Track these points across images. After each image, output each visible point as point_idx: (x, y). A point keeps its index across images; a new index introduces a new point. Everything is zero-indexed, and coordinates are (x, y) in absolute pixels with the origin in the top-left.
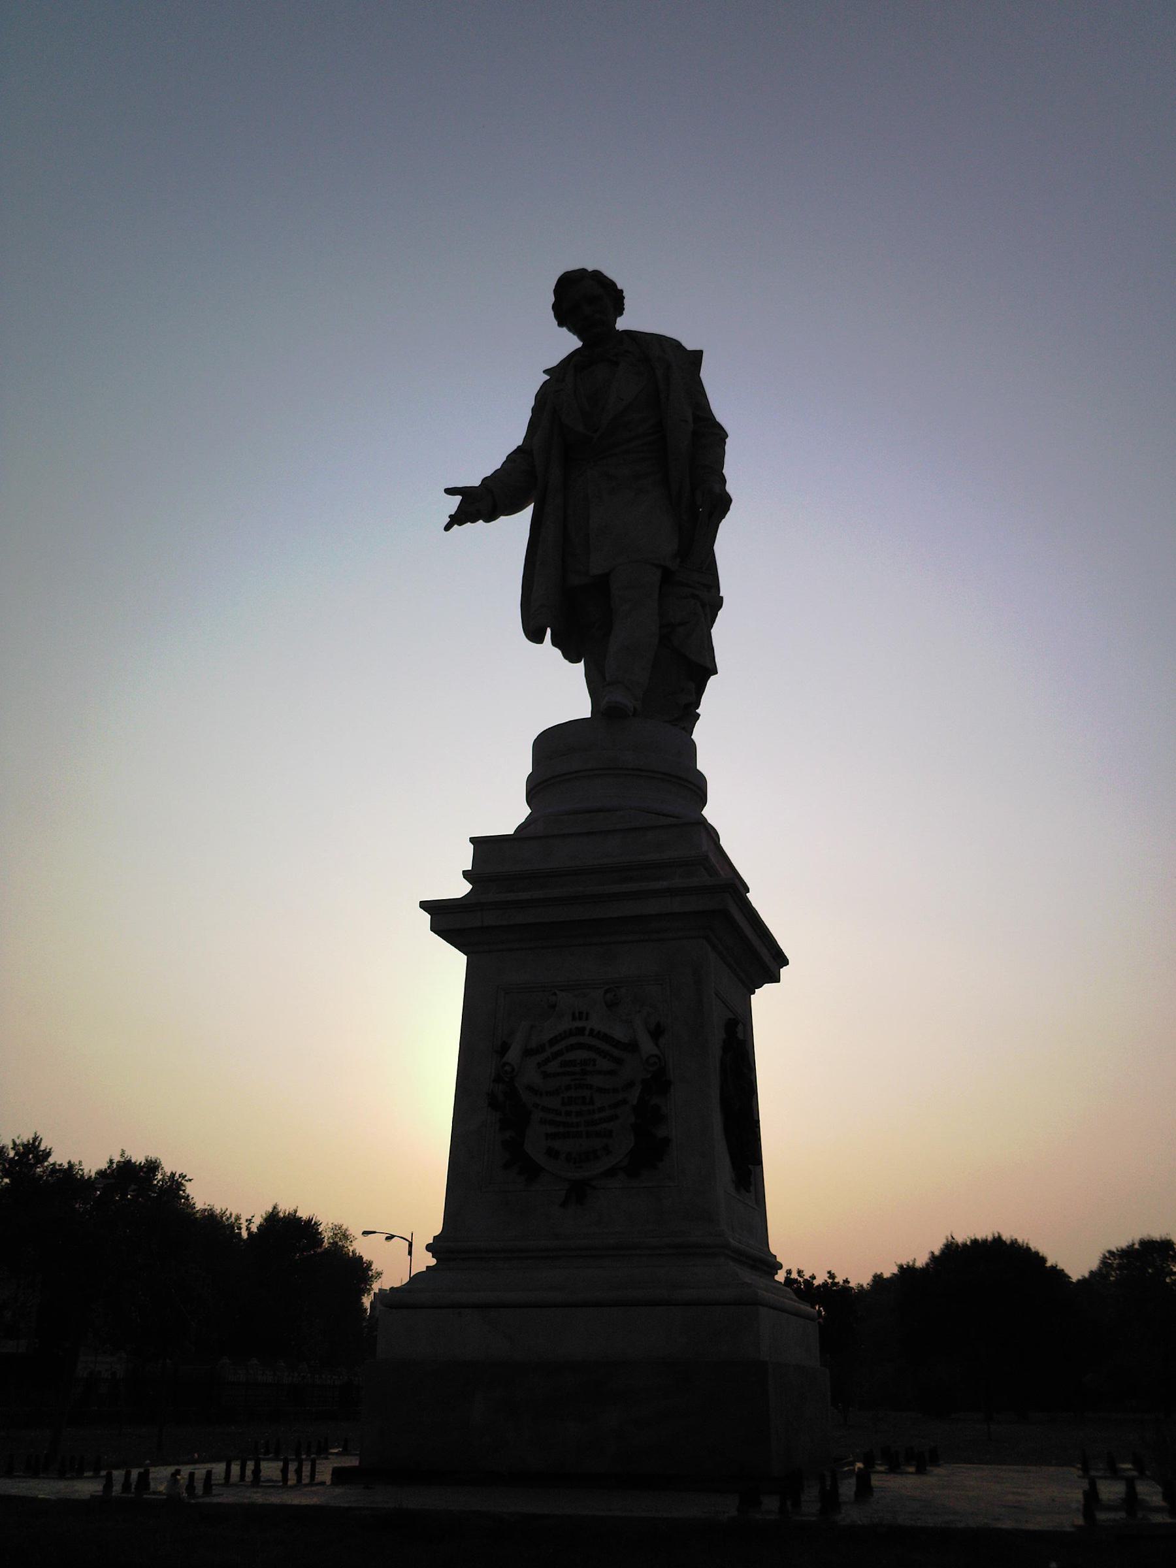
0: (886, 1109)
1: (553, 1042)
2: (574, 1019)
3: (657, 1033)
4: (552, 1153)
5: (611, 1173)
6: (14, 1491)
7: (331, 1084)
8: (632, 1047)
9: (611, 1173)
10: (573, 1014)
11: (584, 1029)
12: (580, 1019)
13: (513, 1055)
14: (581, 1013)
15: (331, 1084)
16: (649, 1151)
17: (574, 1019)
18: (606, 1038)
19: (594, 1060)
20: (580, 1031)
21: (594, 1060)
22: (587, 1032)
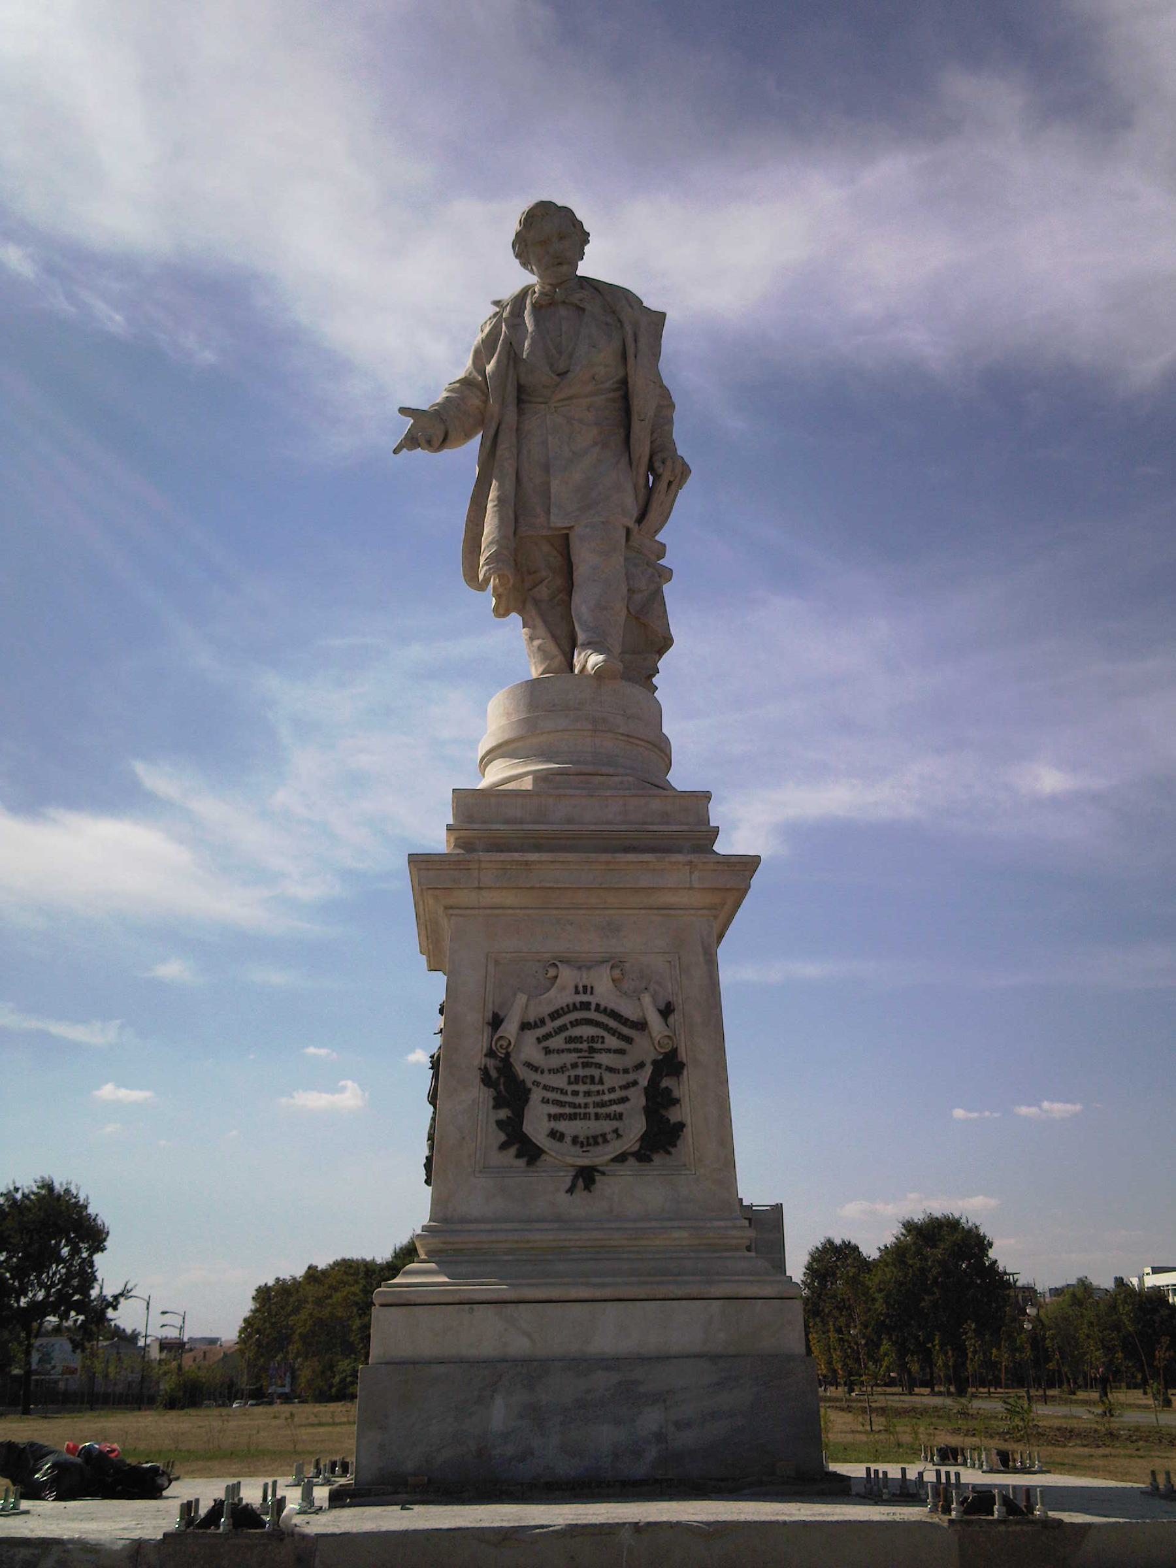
0: (830, 1138)
1: (555, 1015)
2: (577, 992)
3: (666, 1011)
4: (555, 1135)
5: (621, 1158)
6: (1090, 1479)
7: (263, 1157)
8: (641, 1026)
9: (621, 1158)
10: (576, 987)
11: (589, 1003)
12: (585, 992)
13: (510, 1028)
14: (585, 987)
15: (263, 1157)
16: (662, 1135)
17: (577, 992)
18: (614, 1015)
19: (570, 1083)
20: (586, 1006)
21: (570, 1083)
22: (593, 1007)
